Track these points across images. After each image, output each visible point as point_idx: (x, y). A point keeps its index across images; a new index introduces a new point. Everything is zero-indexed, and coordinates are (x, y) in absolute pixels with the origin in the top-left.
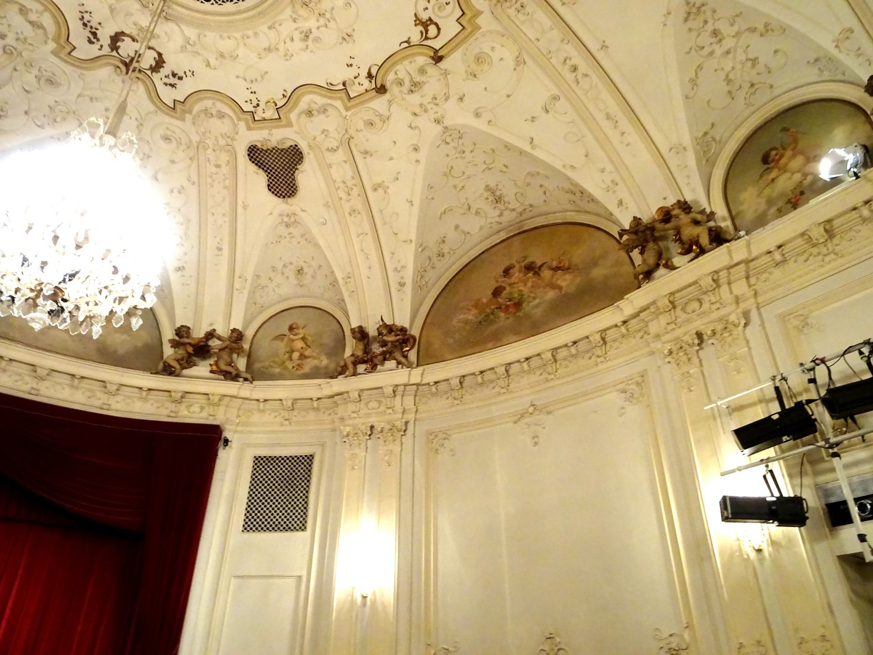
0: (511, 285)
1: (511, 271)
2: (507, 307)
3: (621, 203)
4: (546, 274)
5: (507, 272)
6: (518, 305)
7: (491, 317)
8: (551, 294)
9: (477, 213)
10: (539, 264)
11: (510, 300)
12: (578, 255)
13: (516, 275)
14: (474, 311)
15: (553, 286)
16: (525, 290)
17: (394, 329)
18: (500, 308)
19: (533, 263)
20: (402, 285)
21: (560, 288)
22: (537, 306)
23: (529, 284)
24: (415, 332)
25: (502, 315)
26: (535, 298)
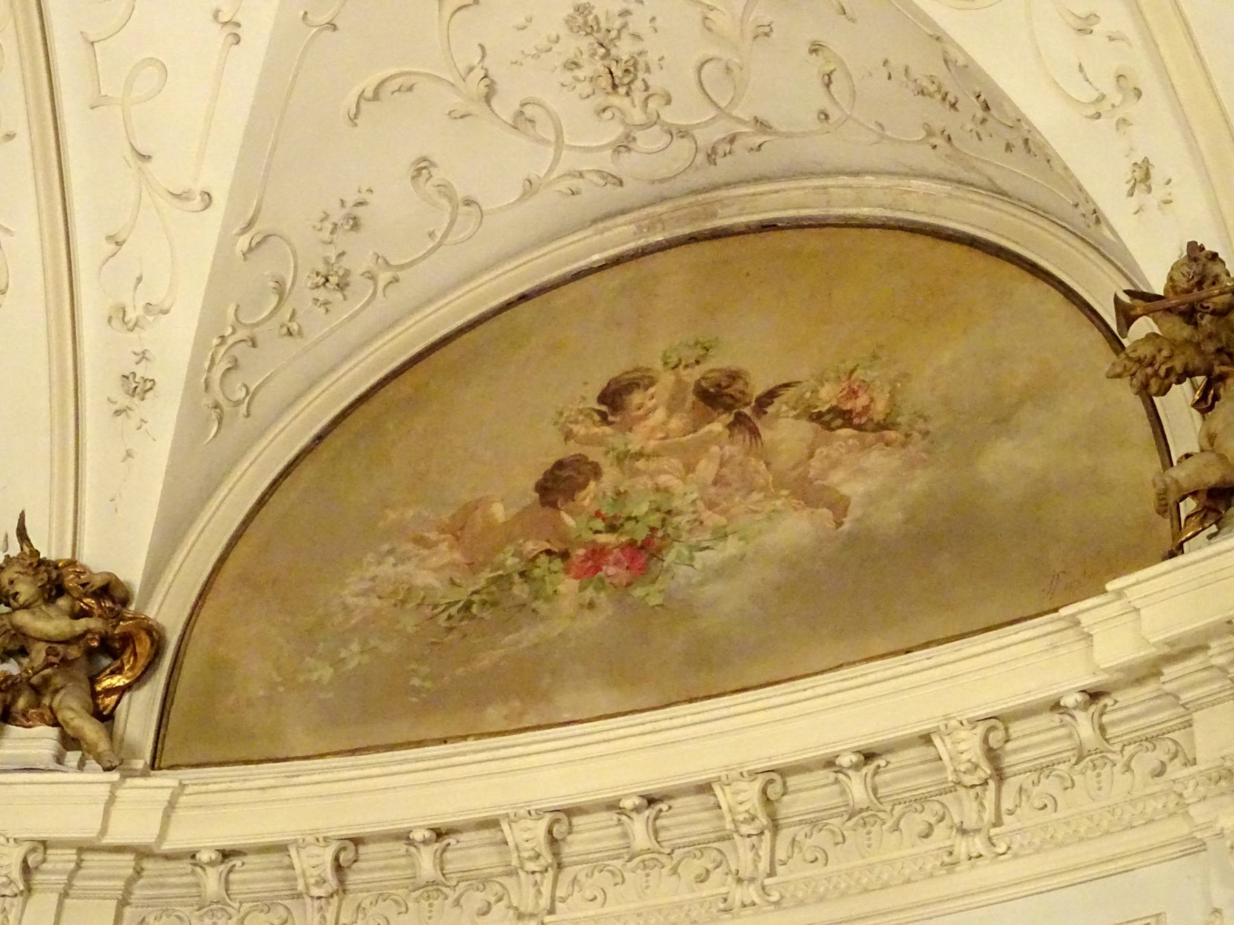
0: (624, 458)
1: (636, 398)
2: (597, 554)
3: (1143, 176)
4: (786, 432)
5: (614, 398)
6: (644, 554)
7: (520, 590)
8: (795, 528)
9: (521, 121)
10: (758, 388)
11: (612, 528)
12: (933, 372)
13: (656, 418)
14: (446, 553)
15: (808, 493)
16: (686, 495)
17: (70, 581)
18: (565, 555)
19: (734, 376)
20: (139, 388)
21: (839, 507)
22: (720, 572)
23: (706, 468)
24: (166, 610)
25: (568, 585)
26: (721, 535)
